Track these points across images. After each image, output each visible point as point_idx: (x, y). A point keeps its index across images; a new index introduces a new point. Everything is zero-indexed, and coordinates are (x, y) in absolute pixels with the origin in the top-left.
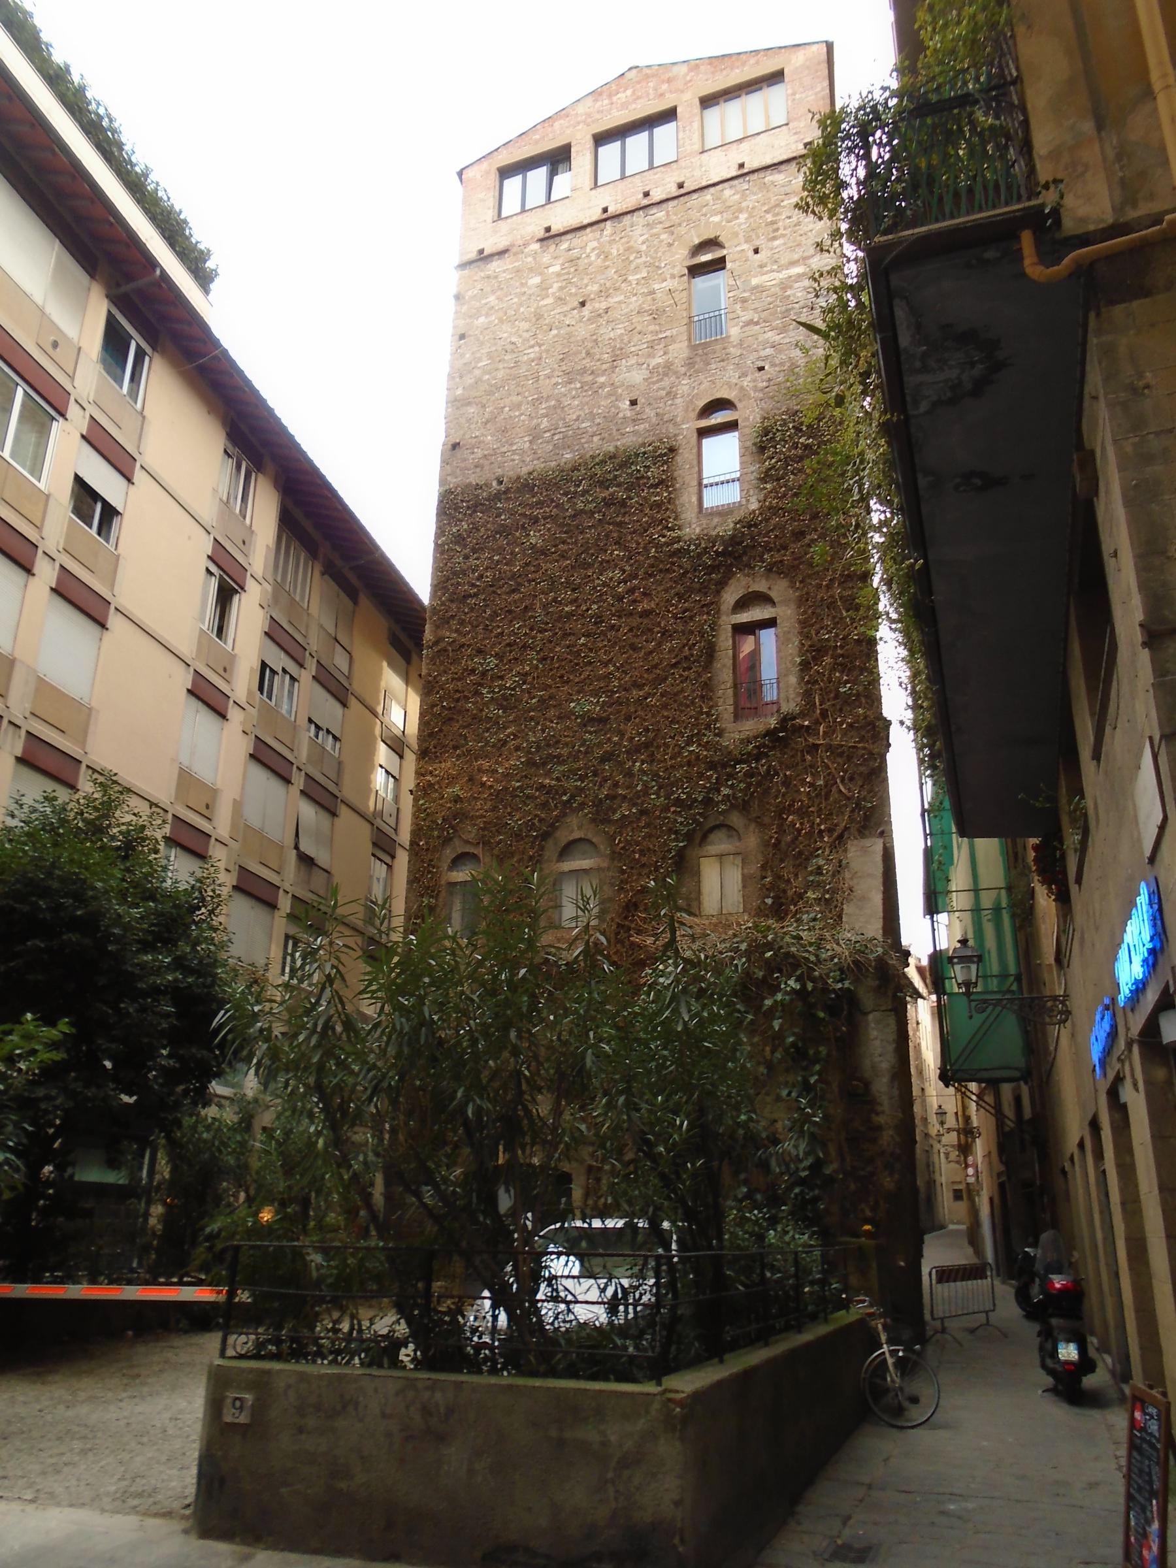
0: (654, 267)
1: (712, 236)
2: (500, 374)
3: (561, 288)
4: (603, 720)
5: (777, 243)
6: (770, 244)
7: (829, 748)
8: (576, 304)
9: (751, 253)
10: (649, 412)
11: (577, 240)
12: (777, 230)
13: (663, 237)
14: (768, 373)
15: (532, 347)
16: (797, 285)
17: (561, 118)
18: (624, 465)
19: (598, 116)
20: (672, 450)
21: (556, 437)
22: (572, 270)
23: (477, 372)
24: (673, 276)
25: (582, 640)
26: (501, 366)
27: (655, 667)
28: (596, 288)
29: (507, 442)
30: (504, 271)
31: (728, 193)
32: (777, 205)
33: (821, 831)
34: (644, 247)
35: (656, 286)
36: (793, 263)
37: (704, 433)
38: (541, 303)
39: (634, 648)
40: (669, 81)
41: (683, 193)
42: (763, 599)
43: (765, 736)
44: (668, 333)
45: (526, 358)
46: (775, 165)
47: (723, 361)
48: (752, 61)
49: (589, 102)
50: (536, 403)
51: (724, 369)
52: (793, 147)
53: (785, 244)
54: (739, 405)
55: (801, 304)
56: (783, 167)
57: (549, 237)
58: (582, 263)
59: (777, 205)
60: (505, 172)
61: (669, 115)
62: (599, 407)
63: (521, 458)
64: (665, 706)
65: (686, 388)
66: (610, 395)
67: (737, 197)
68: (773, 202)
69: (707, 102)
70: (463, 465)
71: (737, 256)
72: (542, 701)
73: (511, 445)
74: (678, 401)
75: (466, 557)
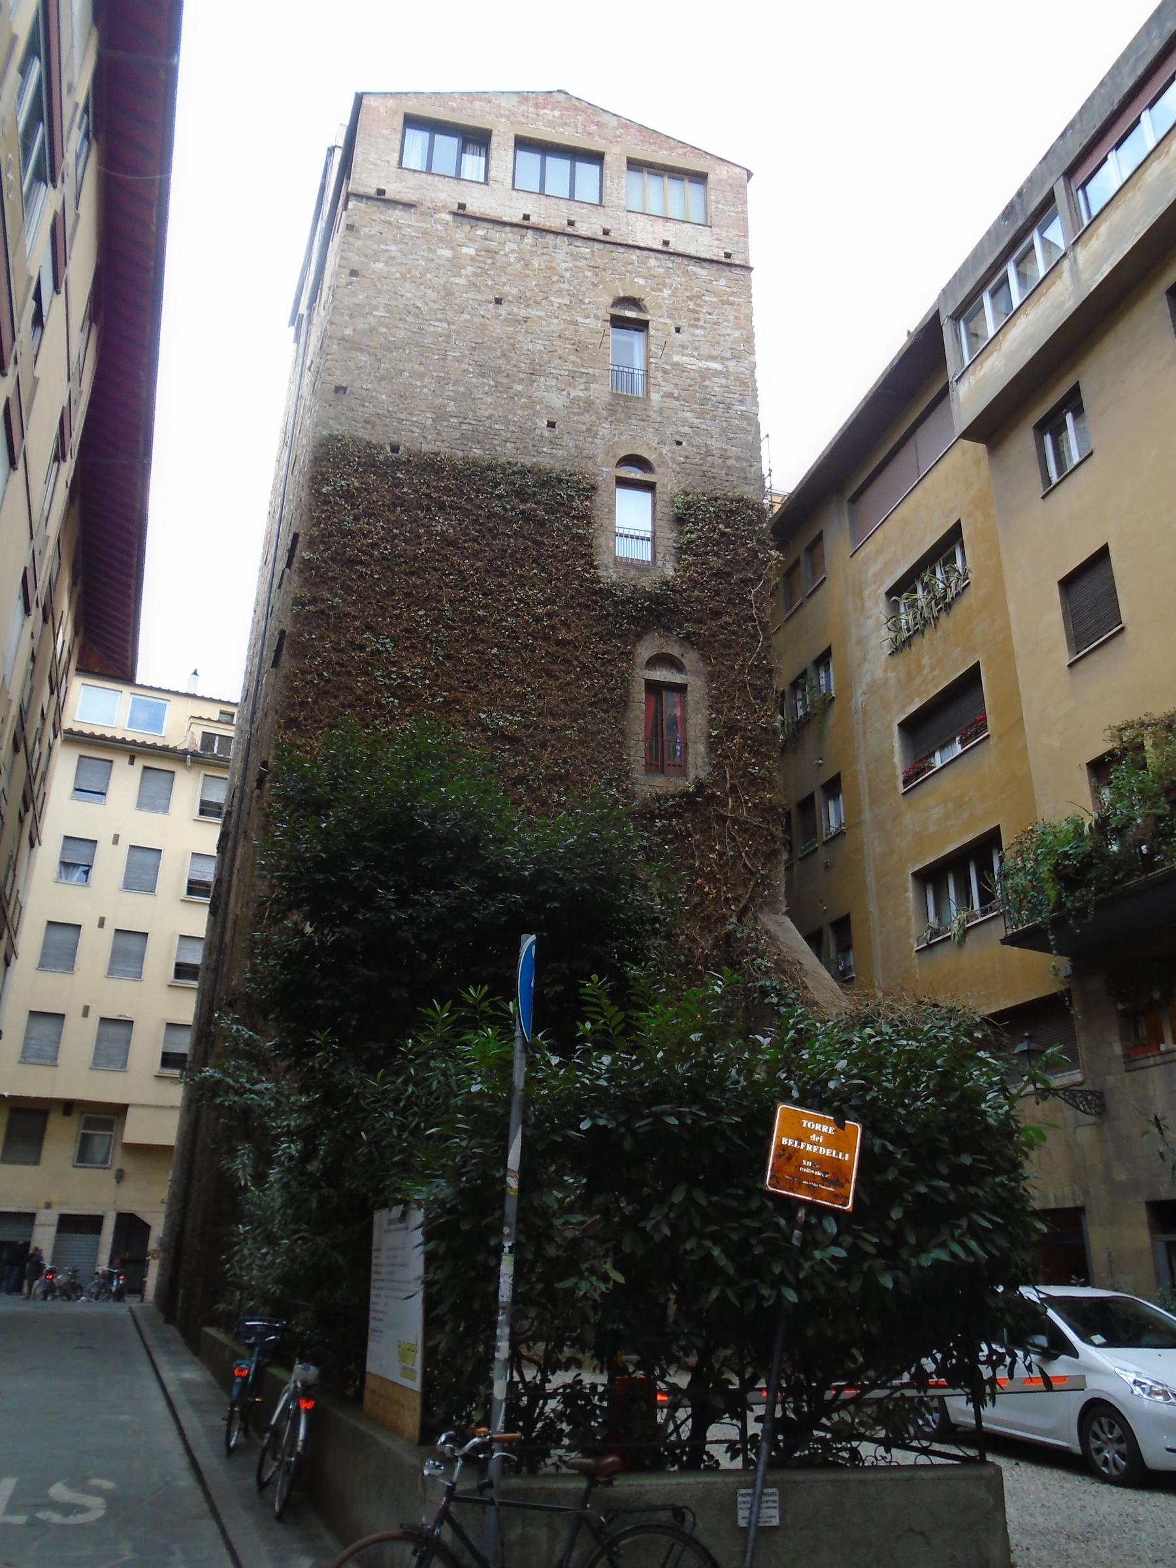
0: (577, 300)
1: (637, 296)
2: (401, 334)
3: (475, 274)
4: (513, 740)
5: (698, 332)
6: (691, 329)
7: (735, 821)
8: (492, 298)
9: (673, 331)
10: (567, 440)
11: (497, 234)
12: (698, 320)
13: (588, 274)
14: (685, 450)
15: (440, 320)
16: (715, 379)
17: (481, 100)
18: (545, 484)
19: (523, 120)
20: (594, 488)
21: (465, 427)
22: (489, 261)
23: (371, 320)
24: (597, 317)
25: (495, 651)
26: (401, 325)
27: (573, 699)
28: (514, 291)
29: (406, 409)
30: (409, 226)
31: (652, 262)
32: (699, 297)
33: (727, 899)
34: (567, 275)
35: (580, 319)
36: (712, 358)
37: (623, 483)
38: (452, 279)
39: (550, 674)
40: (598, 124)
41: (605, 239)
42: (673, 663)
43: (681, 797)
44: (590, 371)
45: (432, 329)
46: (699, 258)
47: (644, 421)
48: (680, 151)
49: (514, 100)
50: (443, 381)
51: (644, 429)
52: (716, 251)
53: (705, 336)
54: (657, 469)
55: (719, 398)
56: (705, 264)
57: (461, 213)
58: (500, 259)
59: (699, 297)
60: (412, 122)
61: (596, 158)
62: (515, 414)
63: (420, 431)
64: (582, 743)
65: (606, 432)
66: (525, 407)
67: (661, 270)
68: (694, 293)
69: (634, 165)
70: (350, 414)
71: (660, 327)
72: (446, 702)
73: (411, 414)
74: (598, 441)
75: (356, 519)
